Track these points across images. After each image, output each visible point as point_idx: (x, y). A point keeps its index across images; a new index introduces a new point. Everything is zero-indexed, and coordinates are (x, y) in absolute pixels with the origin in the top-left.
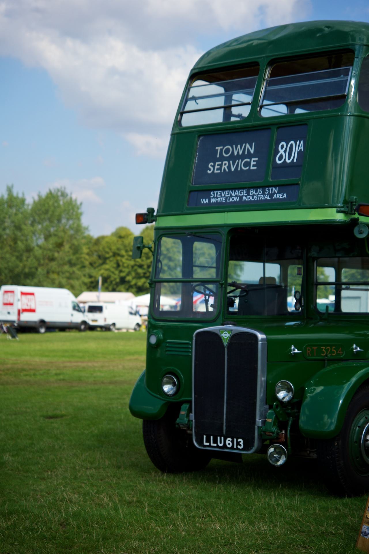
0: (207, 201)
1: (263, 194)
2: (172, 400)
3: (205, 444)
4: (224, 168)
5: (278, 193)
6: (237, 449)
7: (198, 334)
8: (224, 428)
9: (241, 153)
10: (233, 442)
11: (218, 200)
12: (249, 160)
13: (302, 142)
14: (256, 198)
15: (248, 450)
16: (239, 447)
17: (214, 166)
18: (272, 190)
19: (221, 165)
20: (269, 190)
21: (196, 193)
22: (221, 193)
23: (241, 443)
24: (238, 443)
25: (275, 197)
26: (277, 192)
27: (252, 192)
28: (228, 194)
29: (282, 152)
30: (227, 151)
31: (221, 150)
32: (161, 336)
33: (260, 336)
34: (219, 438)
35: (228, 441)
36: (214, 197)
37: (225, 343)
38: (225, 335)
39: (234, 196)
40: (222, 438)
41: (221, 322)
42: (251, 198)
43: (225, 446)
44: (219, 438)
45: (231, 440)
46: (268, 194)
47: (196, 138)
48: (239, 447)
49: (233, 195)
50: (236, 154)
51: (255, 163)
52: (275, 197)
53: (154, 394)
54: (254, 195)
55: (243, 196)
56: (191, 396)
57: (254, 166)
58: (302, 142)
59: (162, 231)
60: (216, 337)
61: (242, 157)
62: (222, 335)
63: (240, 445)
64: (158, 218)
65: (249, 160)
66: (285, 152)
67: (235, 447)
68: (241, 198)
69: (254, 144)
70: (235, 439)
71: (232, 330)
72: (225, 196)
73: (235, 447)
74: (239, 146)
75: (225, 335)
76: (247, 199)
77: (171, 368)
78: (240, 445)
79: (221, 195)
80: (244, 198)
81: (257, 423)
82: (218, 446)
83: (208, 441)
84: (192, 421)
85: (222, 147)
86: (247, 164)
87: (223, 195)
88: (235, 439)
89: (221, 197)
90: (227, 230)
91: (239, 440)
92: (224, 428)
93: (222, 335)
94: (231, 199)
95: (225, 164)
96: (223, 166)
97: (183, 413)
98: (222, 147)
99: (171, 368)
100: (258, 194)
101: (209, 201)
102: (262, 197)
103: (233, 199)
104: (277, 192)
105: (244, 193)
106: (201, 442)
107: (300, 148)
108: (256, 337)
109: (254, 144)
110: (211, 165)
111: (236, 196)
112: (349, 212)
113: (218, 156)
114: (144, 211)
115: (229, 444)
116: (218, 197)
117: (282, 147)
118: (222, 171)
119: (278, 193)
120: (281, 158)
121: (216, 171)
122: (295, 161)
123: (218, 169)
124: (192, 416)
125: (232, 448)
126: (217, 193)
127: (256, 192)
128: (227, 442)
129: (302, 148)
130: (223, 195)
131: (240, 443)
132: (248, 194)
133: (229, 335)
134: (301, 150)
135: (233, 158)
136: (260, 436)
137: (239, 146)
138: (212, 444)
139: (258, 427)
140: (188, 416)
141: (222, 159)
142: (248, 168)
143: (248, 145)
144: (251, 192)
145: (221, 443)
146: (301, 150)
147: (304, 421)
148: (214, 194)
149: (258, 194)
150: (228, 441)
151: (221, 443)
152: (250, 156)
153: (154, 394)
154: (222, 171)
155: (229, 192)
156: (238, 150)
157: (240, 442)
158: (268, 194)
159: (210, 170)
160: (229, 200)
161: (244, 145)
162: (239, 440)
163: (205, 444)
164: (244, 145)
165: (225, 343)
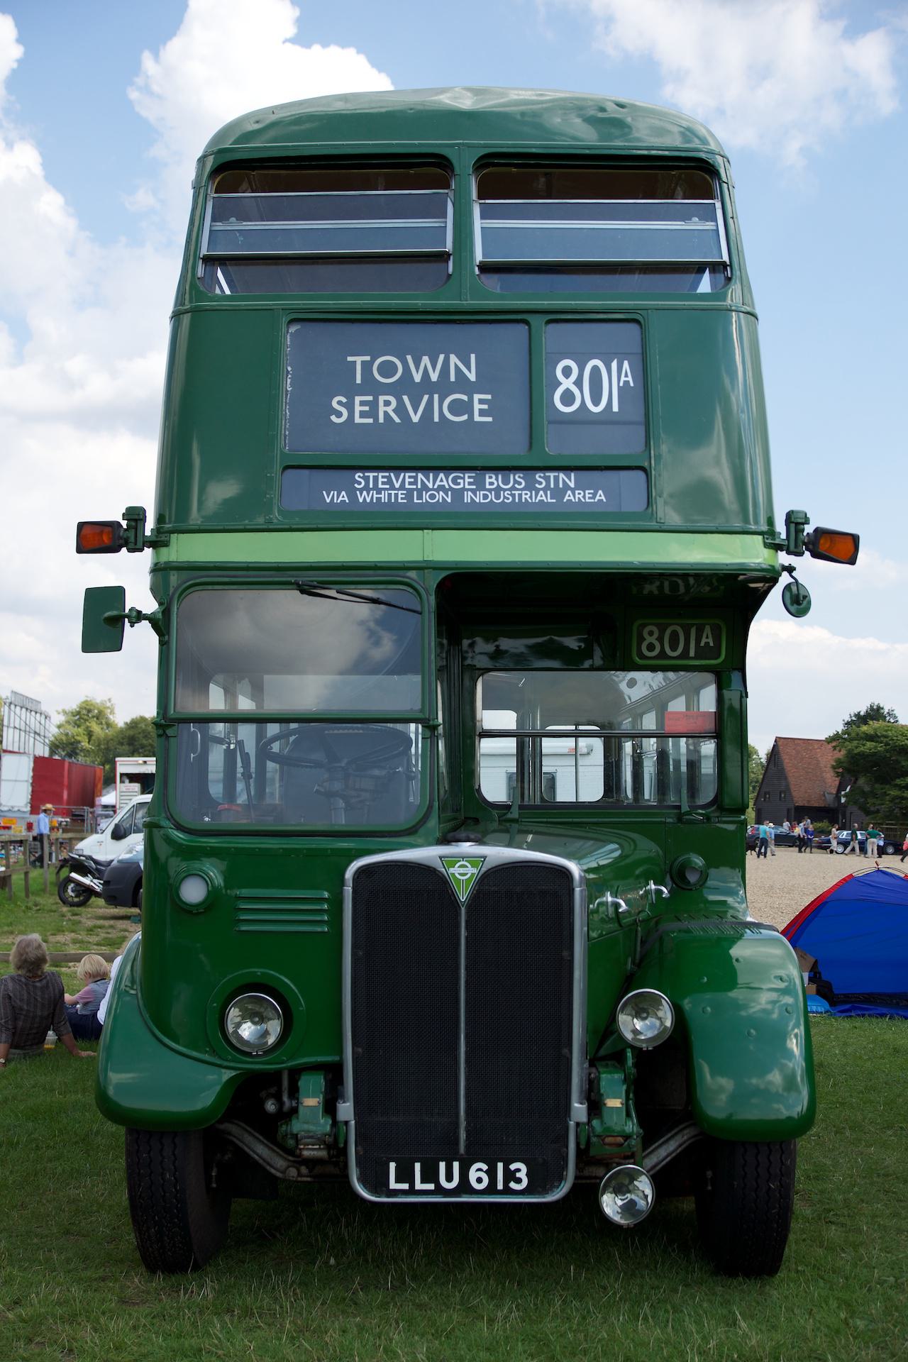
0: (344, 497)
1: (530, 487)
2: (257, 1067)
3: (393, 1185)
4: (386, 413)
5: (576, 488)
6: (507, 1191)
7: (361, 871)
8: (463, 1135)
9: (434, 377)
10: (492, 1173)
11: (384, 497)
12: (465, 398)
13: (626, 365)
14: (506, 498)
15: (545, 1191)
16: (513, 1185)
17: (350, 406)
18: (556, 479)
19: (374, 405)
20: (547, 479)
21: (306, 472)
22: (389, 478)
23: (522, 1175)
24: (510, 1176)
25: (569, 496)
26: (572, 485)
27: (491, 480)
28: (415, 483)
29: (567, 384)
30: (387, 369)
31: (367, 367)
32: (219, 880)
33: (574, 868)
34: (442, 1165)
35: (477, 1173)
36: (367, 488)
37: (463, 896)
38: (462, 870)
39: (437, 489)
40: (456, 1165)
41: (438, 834)
42: (492, 496)
43: (465, 1186)
44: (442, 1165)
45: (485, 1167)
46: (545, 490)
47: (284, 326)
48: (513, 1185)
49: (430, 486)
50: (417, 378)
51: (485, 407)
52: (569, 496)
53: (195, 1054)
54: (498, 490)
55: (464, 489)
56: (340, 1050)
57: (482, 413)
58: (626, 365)
59: (185, 574)
60: (430, 881)
61: (443, 387)
62: (451, 870)
63: (519, 1181)
64: (174, 536)
65: (465, 398)
66: (578, 382)
67: (500, 1186)
68: (458, 494)
69: (473, 356)
70: (500, 1166)
71: (485, 857)
72: (402, 487)
73: (500, 1186)
74: (426, 360)
75: (462, 870)
76: (479, 499)
77: (259, 971)
78: (519, 1181)
79: (390, 482)
80: (468, 497)
81: (573, 1113)
82: (439, 1190)
83: (405, 1174)
84: (346, 1123)
85: (368, 358)
86: (466, 408)
87: (397, 486)
88: (500, 1166)
89: (393, 488)
90: (433, 580)
91: (513, 1167)
92: (463, 1135)
93: (451, 870)
94: (426, 496)
95: (387, 403)
96: (382, 409)
97: (311, 1101)
98: (368, 358)
99: (259, 971)
100: (513, 488)
101: (352, 494)
102: (526, 496)
103: (432, 497)
104: (572, 485)
105: (466, 480)
106: (379, 1184)
107: (623, 378)
108: (565, 873)
109: (473, 356)
110: (339, 403)
111: (441, 488)
112: (792, 548)
113: (359, 381)
114: (114, 514)
115: (479, 1180)
116: (377, 489)
117: (567, 372)
118: (381, 420)
119: (576, 488)
120: (568, 398)
121: (358, 420)
122: (615, 408)
123: (363, 414)
124: (346, 1110)
125: (491, 1189)
126: (376, 479)
127: (506, 482)
128: (473, 1175)
129: (630, 379)
130: (397, 486)
131: (518, 1175)
132: (480, 485)
133: (475, 871)
134: (626, 383)
135: (405, 386)
136: (580, 1153)
137: (426, 360)
138: (419, 1186)
139: (578, 1124)
140: (330, 1108)
141: (371, 386)
142: (465, 417)
143: (453, 359)
144: (488, 480)
145: (449, 1178)
146: (626, 383)
147: (718, 1092)
148: (367, 479)
149: (513, 488)
150: (477, 1173)
151: (449, 1178)
152: (469, 388)
153: (195, 1054)
154: (381, 420)
155: (416, 478)
156: (425, 368)
157: (519, 1170)
158: (545, 490)
159: (339, 415)
160: (420, 497)
161: (442, 357)
162: (513, 1167)
163: (393, 1185)
164: (442, 357)
165: (463, 896)
